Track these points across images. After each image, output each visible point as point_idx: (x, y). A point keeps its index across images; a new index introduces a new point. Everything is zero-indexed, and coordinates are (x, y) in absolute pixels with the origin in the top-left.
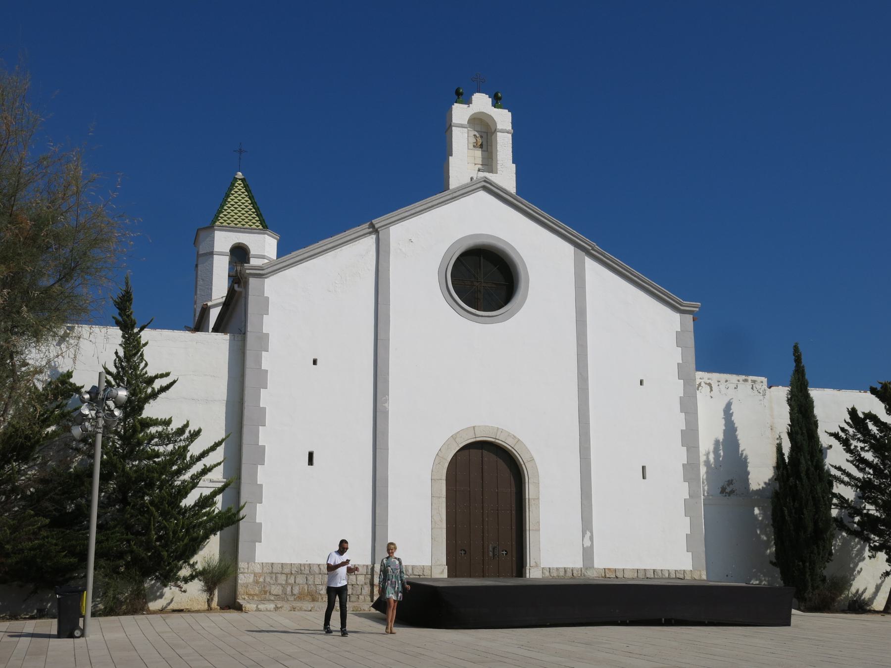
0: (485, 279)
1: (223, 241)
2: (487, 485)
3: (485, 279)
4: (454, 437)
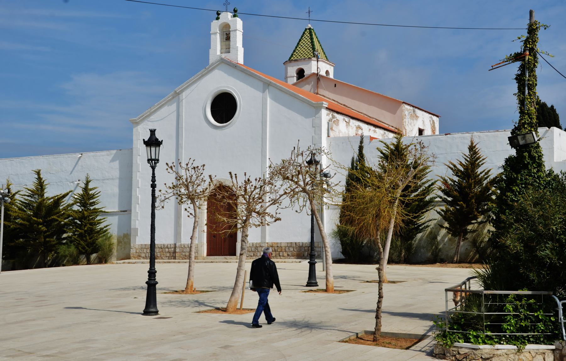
1: (215, 26)
3: (224, 107)
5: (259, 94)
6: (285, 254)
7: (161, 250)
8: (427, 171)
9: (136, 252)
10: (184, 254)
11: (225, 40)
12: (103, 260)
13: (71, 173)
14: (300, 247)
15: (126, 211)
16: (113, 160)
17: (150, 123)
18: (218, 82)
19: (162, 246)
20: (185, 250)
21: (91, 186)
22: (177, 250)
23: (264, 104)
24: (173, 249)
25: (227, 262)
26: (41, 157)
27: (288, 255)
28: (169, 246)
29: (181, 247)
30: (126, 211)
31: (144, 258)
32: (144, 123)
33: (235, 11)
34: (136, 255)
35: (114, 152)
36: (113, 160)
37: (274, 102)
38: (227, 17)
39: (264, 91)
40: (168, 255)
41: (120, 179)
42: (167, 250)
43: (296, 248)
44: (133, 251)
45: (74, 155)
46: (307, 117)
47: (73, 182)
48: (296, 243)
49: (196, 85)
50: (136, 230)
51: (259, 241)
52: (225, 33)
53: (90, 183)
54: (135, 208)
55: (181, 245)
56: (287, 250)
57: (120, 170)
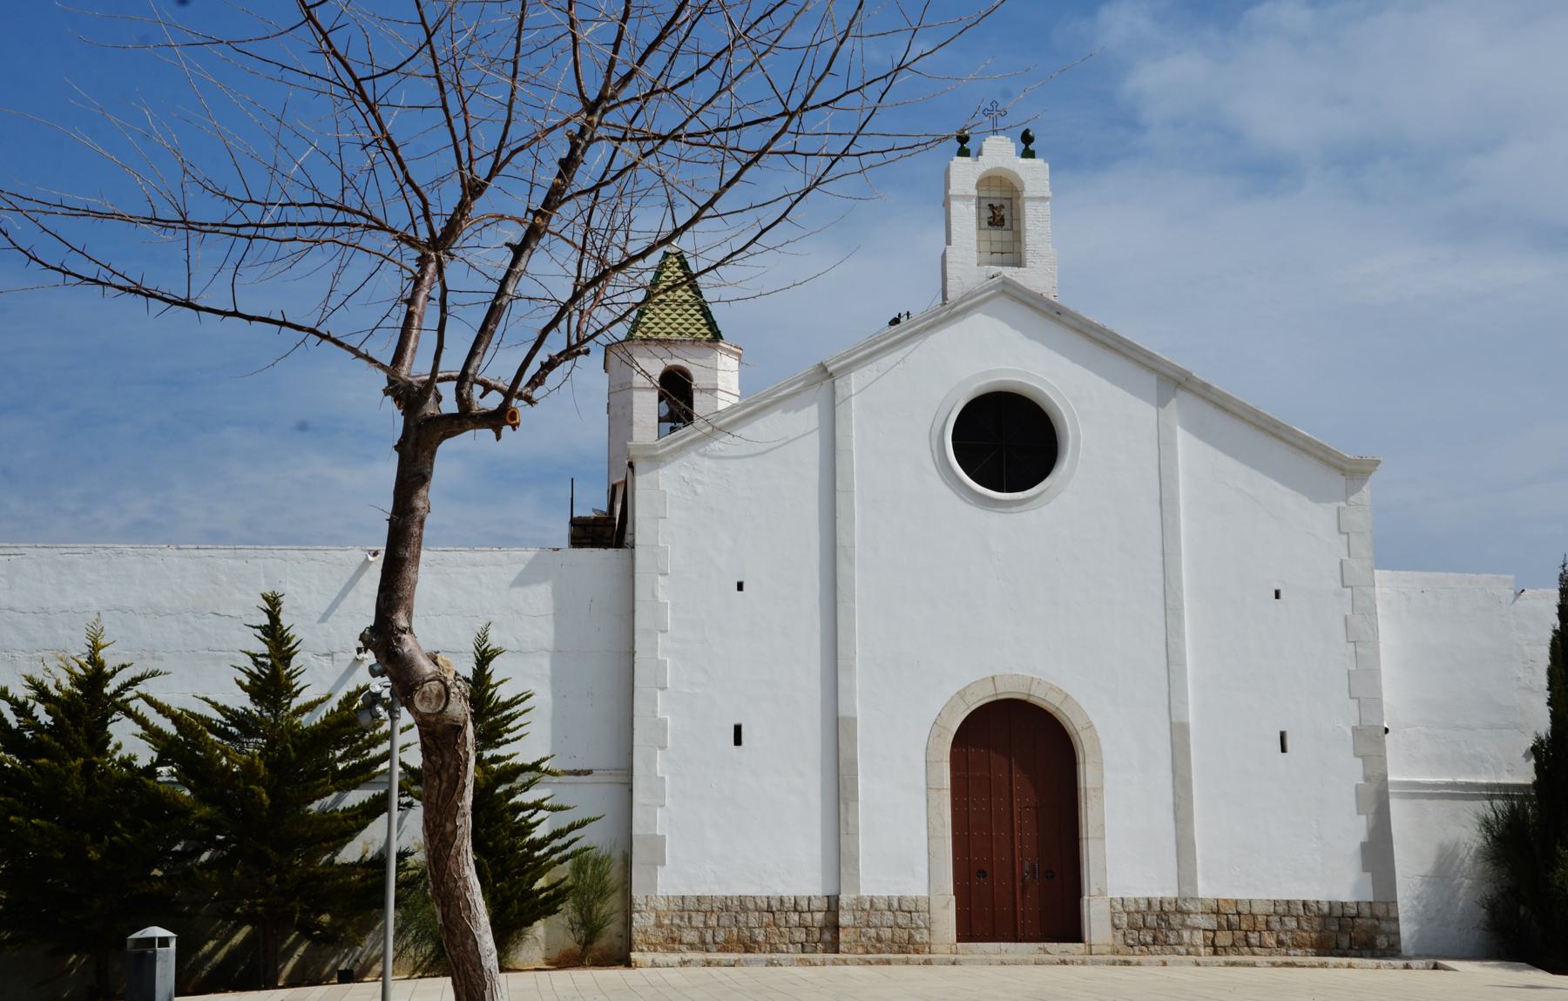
0: (1006, 442)
2: (1018, 788)
4: (961, 694)
5: (1145, 411)
6: (1270, 940)
7: (767, 918)
8: (215, 715)
9: (659, 925)
10: (872, 932)
11: (985, 224)
12: (621, 958)
13: (324, 618)
14: (1325, 917)
15: (588, 772)
16: (522, 581)
17: (707, 462)
18: (994, 354)
19: (775, 905)
20: (875, 920)
21: (497, 669)
22: (845, 919)
23: (1164, 445)
24: (819, 916)
25: (1127, 963)
26: (171, 551)
27: (1280, 943)
28: (804, 904)
29: (858, 906)
30: (588, 772)
31: (692, 947)
32: (683, 461)
33: (1027, 138)
34: (658, 936)
35: (530, 553)
36: (522, 581)
37: (1195, 440)
38: (999, 152)
39: (1161, 403)
40: (800, 935)
41: (558, 653)
42: (794, 917)
43: (1309, 920)
44: (642, 921)
45: (339, 554)
46: (1316, 497)
47: (331, 655)
48: (1305, 904)
49: (907, 350)
50: (658, 844)
51: (1171, 892)
52: (985, 203)
53: (492, 665)
54: (651, 762)
55: (859, 900)
56: (1275, 925)
57: (558, 624)
